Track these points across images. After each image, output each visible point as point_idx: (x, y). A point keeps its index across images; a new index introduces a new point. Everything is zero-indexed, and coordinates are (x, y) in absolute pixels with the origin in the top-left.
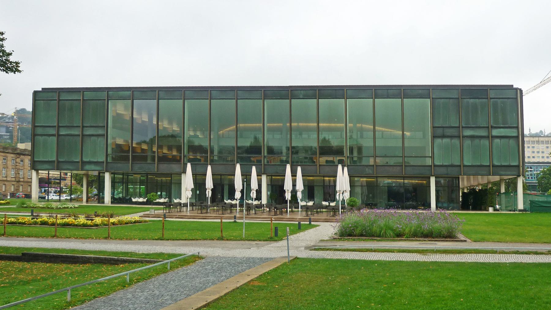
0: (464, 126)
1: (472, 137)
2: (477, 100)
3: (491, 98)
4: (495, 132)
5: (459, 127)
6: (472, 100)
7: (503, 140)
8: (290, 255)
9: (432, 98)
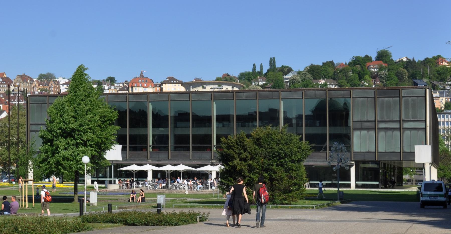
0: (379, 120)
1: (386, 129)
2: (391, 99)
3: (403, 97)
4: (406, 125)
6: (387, 99)
7: (413, 132)
8: (19, 122)
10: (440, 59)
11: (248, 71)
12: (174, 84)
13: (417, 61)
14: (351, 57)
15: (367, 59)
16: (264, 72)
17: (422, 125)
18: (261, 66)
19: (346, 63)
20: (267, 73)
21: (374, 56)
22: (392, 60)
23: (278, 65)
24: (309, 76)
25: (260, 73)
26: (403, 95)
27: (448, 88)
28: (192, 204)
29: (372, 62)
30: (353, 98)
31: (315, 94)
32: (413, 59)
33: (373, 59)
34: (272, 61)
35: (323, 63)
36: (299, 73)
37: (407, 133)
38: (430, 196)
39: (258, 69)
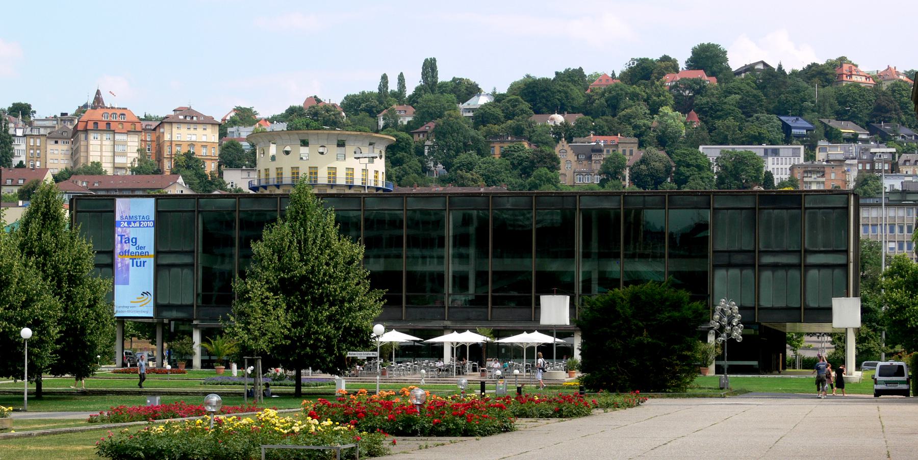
0: (762, 249)
1: (775, 267)
4: (812, 259)
5: (754, 251)
7: (824, 272)
9: (714, 209)
10: (846, 67)
11: (367, 90)
12: (192, 126)
13: (788, 71)
14: (628, 60)
15: (668, 64)
16: (409, 91)
17: (839, 259)
18: (401, 79)
19: (613, 75)
20: (414, 95)
21: (682, 57)
22: (729, 68)
23: (444, 76)
24: (525, 106)
25: (398, 96)
26: (807, 206)
27: (864, 137)
28: (22, 439)
29: (677, 71)
30: (714, 209)
31: (644, 201)
32: (780, 67)
33: (682, 65)
34: (430, 67)
35: (557, 73)
36: (498, 98)
37: (813, 273)
38: (887, 383)
39: (393, 86)
